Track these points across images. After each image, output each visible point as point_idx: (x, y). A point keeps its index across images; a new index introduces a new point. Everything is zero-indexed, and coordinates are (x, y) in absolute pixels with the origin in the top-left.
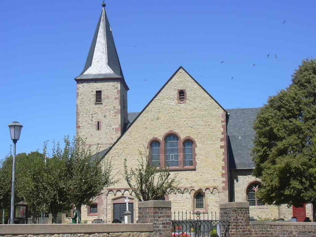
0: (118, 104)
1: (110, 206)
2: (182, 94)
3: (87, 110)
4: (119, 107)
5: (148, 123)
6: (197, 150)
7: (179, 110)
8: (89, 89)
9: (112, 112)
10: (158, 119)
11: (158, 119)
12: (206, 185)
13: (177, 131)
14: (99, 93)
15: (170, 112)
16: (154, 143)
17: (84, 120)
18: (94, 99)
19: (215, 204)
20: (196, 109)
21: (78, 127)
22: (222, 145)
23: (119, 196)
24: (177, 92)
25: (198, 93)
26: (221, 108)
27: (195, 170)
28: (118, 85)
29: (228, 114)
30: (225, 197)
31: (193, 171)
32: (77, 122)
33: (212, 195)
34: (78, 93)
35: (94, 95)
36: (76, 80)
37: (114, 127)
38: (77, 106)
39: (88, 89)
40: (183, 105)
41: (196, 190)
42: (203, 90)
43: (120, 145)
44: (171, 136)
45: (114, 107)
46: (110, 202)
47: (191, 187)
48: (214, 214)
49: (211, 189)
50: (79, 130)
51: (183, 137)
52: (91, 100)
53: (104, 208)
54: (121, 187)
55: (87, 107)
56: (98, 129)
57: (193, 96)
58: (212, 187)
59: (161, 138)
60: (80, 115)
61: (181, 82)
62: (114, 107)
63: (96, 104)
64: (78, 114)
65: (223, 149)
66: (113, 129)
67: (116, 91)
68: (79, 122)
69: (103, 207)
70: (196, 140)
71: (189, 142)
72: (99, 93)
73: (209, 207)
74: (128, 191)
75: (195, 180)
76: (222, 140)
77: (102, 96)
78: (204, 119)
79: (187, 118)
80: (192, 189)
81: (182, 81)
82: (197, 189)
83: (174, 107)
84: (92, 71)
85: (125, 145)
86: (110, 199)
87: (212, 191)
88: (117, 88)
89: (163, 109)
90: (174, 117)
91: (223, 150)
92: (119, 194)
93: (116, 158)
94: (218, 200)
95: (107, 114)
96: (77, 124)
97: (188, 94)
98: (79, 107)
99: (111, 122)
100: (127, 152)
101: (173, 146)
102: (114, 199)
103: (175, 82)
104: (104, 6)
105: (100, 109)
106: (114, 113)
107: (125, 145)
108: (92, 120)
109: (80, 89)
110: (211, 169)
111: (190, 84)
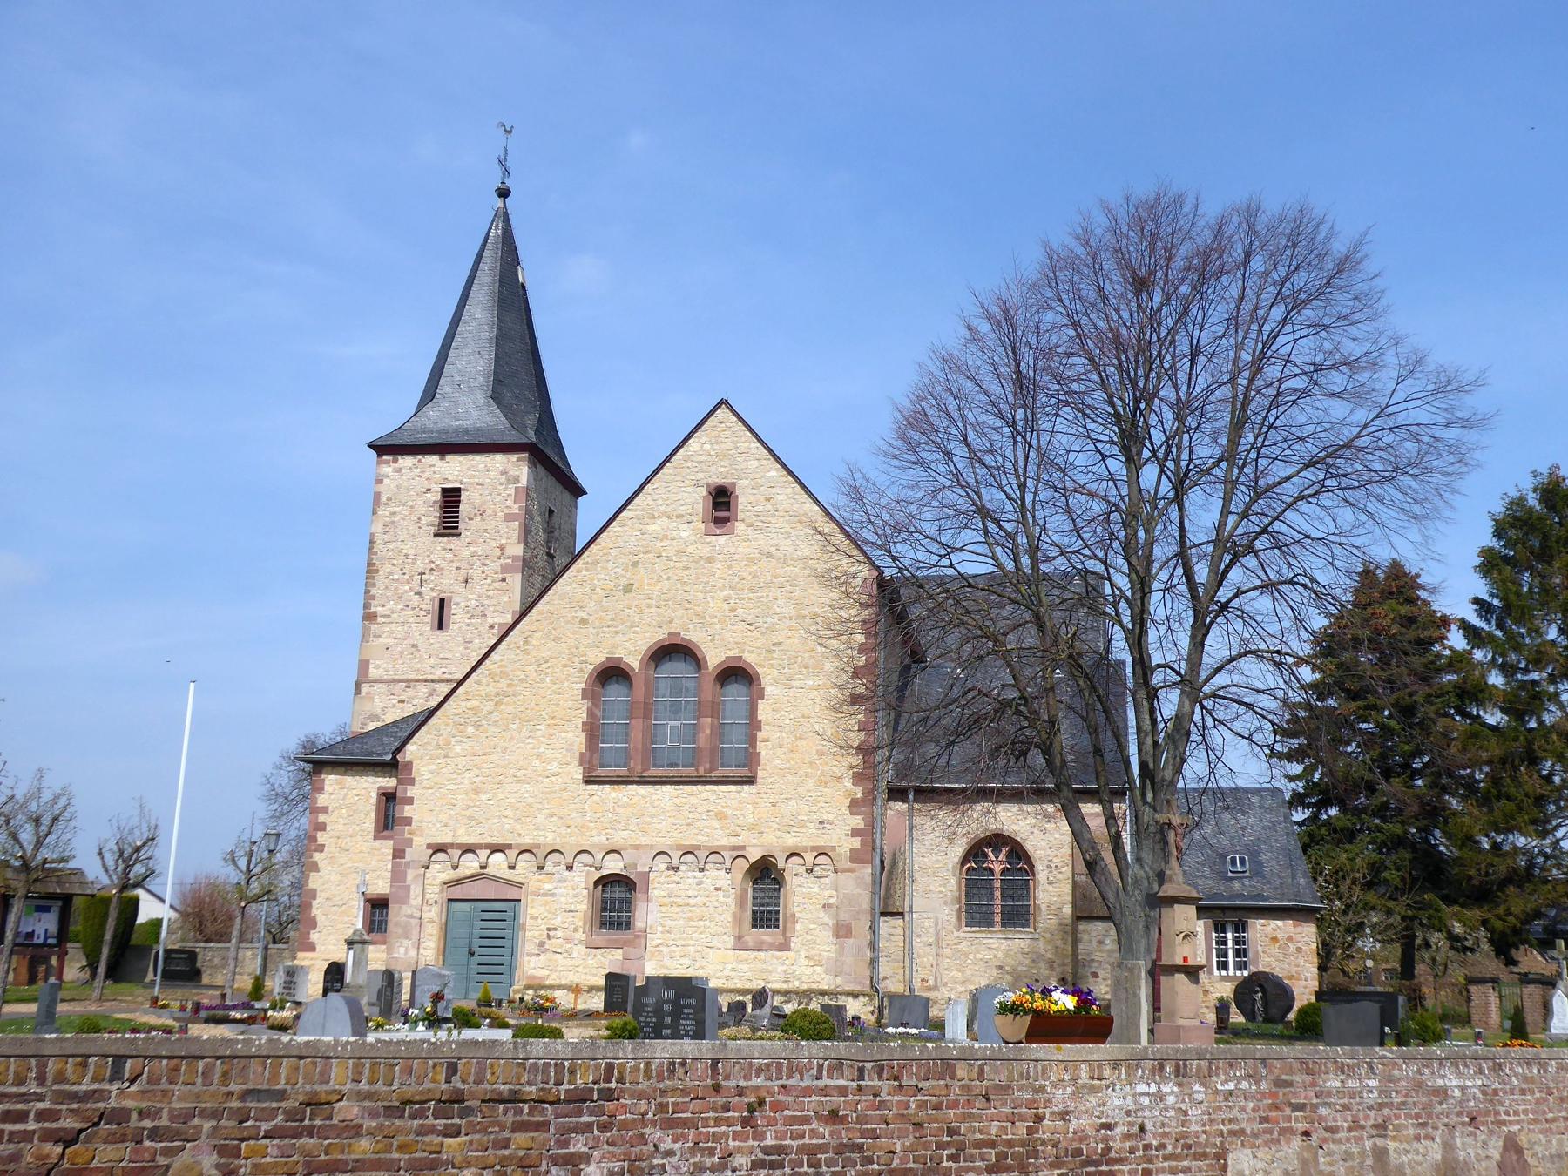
1: (435, 909)
2: (721, 500)
4: (518, 550)
6: (764, 710)
7: (710, 560)
9: (495, 566)
10: (628, 589)
11: (628, 589)
12: (791, 841)
13: (694, 635)
14: (451, 497)
16: (611, 674)
17: (392, 592)
18: (432, 517)
19: (822, 914)
20: (769, 555)
21: (370, 617)
23: (468, 872)
25: (780, 498)
27: (751, 781)
28: (519, 468)
30: (859, 890)
31: (746, 787)
32: (369, 597)
33: (811, 879)
34: (377, 496)
36: (371, 446)
38: (372, 542)
39: (414, 483)
40: (722, 540)
41: (752, 860)
43: (484, 680)
44: (672, 651)
45: (502, 548)
46: (434, 892)
47: (735, 848)
48: (484, 969)
49: (702, 854)
50: (374, 627)
51: (714, 658)
53: (411, 916)
54: (448, 840)
55: (407, 548)
56: (440, 627)
57: (761, 509)
58: (813, 848)
60: (381, 576)
61: (721, 456)
62: (502, 548)
63: (436, 535)
64: (371, 570)
66: (492, 627)
68: (373, 598)
69: (406, 910)
70: (760, 671)
71: (736, 674)
72: (451, 497)
73: (798, 927)
75: (751, 820)
77: (461, 508)
79: (731, 588)
82: (755, 855)
84: (438, 420)
85: (503, 683)
86: (438, 881)
87: (541, 861)
88: (517, 480)
92: (470, 864)
93: (470, 729)
94: (831, 901)
95: (476, 573)
96: (366, 606)
98: (378, 547)
100: (510, 709)
101: (679, 694)
102: (451, 883)
105: (449, 556)
108: (419, 594)
109: (386, 481)
110: (811, 782)
111: (753, 464)
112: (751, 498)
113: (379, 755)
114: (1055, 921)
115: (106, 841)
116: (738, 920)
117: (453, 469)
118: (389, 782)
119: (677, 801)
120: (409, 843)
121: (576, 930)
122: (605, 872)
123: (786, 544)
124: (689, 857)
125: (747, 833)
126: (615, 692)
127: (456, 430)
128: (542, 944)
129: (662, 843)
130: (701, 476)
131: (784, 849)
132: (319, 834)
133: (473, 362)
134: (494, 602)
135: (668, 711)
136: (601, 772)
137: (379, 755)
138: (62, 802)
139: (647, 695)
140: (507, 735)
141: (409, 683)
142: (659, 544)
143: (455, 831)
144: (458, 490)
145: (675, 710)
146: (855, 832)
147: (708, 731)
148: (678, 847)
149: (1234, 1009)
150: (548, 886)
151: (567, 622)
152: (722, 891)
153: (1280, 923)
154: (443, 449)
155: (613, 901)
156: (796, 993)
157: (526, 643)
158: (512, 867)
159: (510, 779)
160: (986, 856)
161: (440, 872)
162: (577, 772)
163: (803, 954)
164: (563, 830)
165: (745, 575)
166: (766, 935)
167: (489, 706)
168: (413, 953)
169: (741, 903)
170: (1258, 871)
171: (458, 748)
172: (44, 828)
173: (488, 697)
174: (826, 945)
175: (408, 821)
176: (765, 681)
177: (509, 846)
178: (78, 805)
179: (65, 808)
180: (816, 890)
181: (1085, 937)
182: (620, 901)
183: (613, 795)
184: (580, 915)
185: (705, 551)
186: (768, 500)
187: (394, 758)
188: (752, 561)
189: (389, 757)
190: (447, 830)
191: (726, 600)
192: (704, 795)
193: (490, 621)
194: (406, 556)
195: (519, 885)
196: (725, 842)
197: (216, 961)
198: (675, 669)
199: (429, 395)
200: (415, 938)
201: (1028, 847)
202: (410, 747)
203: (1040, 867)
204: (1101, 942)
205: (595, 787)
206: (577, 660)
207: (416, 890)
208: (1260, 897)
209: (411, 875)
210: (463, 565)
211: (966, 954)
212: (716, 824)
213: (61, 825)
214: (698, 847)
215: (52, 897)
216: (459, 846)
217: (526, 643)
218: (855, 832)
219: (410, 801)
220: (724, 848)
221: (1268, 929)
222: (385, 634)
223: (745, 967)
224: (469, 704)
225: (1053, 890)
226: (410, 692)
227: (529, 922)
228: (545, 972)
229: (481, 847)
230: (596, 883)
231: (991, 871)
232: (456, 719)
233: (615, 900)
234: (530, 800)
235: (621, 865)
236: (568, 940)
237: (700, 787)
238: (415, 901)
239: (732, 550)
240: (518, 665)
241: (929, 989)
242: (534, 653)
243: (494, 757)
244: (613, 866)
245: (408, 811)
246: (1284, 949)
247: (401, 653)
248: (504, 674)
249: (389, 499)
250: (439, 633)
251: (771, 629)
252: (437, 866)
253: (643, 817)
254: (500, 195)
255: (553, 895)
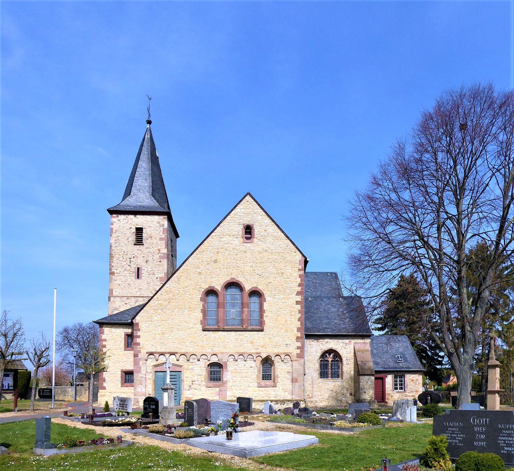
0: (164, 246)
1: (151, 374)
2: (248, 230)
3: (124, 252)
4: (165, 251)
5: (202, 267)
6: (266, 306)
7: (245, 252)
8: (126, 224)
9: (157, 256)
10: (215, 261)
11: (215, 261)
12: (276, 351)
13: (240, 279)
14: (139, 231)
15: (231, 253)
16: (211, 292)
17: (119, 265)
18: (133, 238)
19: (287, 375)
20: (266, 251)
22: (298, 300)
23: (162, 362)
24: (242, 227)
25: (269, 230)
26: (298, 252)
27: (262, 330)
28: (163, 221)
29: (308, 260)
30: (299, 367)
31: (260, 333)
32: (111, 267)
33: (283, 363)
35: (134, 232)
37: (159, 276)
38: (111, 246)
40: (249, 245)
41: (263, 357)
42: (276, 227)
45: (159, 250)
46: (150, 369)
47: (257, 353)
50: (114, 277)
51: (248, 287)
52: (130, 239)
53: (142, 377)
54: (154, 351)
55: (124, 249)
56: (138, 278)
58: (284, 353)
59: (219, 287)
61: (248, 214)
62: (159, 250)
63: (135, 245)
64: (111, 256)
65: (300, 306)
66: (157, 278)
67: (162, 230)
68: (113, 266)
69: (140, 375)
70: (264, 292)
71: (256, 293)
72: (139, 231)
73: (279, 379)
74: (164, 355)
75: (262, 344)
76: (298, 294)
77: (144, 235)
78: (277, 265)
80: (258, 355)
81: (248, 211)
82: (264, 356)
83: (238, 248)
84: (131, 202)
85: (171, 295)
86: (151, 365)
89: (222, 248)
90: (236, 260)
91: (299, 307)
93: (160, 311)
95: (150, 259)
96: (110, 269)
97: (257, 230)
99: (155, 269)
100: (174, 304)
101: (234, 300)
102: (156, 366)
103: (241, 214)
104: (149, 122)
105: (140, 252)
106: (158, 258)
107: (171, 295)
108: (130, 266)
109: (114, 224)
110: (283, 331)
111: (260, 217)
112: (259, 230)
113: (126, 321)
114: (348, 376)
115: (29, 349)
116: (258, 377)
117: (140, 220)
118: (129, 331)
119: (236, 337)
120: (140, 352)
121: (202, 381)
122: (211, 362)
123: (272, 247)
124: (241, 357)
125: (261, 348)
126: (212, 299)
127: (140, 206)
128: (190, 386)
129: (232, 352)
130: (241, 221)
131: (274, 354)
132: (104, 349)
133: (143, 182)
134: (157, 269)
135: (232, 305)
136: (207, 327)
137: (126, 321)
138: (18, 326)
139: (224, 300)
140: (173, 314)
141: (128, 297)
142: (226, 245)
143: (156, 347)
144: (142, 229)
145: (233, 305)
146: (298, 348)
147: (246, 313)
148: (237, 353)
149: (418, 402)
150: (191, 367)
151: (193, 273)
152: (254, 368)
153: (414, 375)
154: (135, 213)
155: (214, 371)
156: (280, 401)
157: (179, 280)
158: (178, 360)
159: (174, 328)
160: (326, 356)
161: (152, 362)
162: (200, 327)
163: (281, 388)
164: (196, 347)
165: (258, 258)
166: (268, 382)
167: (166, 303)
168: (144, 390)
169: (259, 371)
170: (406, 360)
171: (155, 318)
172: (9, 339)
173: (165, 300)
174: (289, 385)
175: (139, 344)
176: (266, 296)
177: (177, 353)
178: (26, 328)
179: (19, 330)
180: (285, 367)
181: (362, 381)
182: (217, 372)
183: (213, 335)
184: (203, 376)
185: (243, 248)
186: (265, 231)
187: (132, 322)
188: (260, 253)
189: (130, 321)
190: (153, 347)
191: (251, 267)
192: (246, 335)
193: (156, 276)
194: (124, 252)
195: (181, 366)
196: (253, 351)
197: (59, 392)
198: (233, 291)
199: (128, 192)
200: (144, 385)
201: (340, 353)
202: (137, 317)
203: (344, 359)
204: (367, 382)
205: (207, 332)
206: (198, 287)
207: (143, 369)
208: (408, 368)
209: (141, 363)
210: (145, 256)
211: (321, 387)
212: (250, 345)
213: (18, 337)
214: (244, 353)
215: (11, 370)
216: (158, 353)
217: (179, 280)
218: (298, 348)
219: (139, 337)
220: (253, 353)
221: (411, 377)
222: (118, 280)
223: (262, 393)
224: (159, 302)
225: (348, 367)
226: (129, 301)
227: (185, 379)
228: (191, 396)
229: (166, 353)
230: (208, 365)
231: (328, 361)
232: (154, 307)
233: (216, 371)
234: (183, 337)
235: (217, 359)
236: (199, 385)
237: (244, 332)
238: (143, 372)
239: (253, 248)
240: (176, 288)
241: (310, 398)
242: (182, 284)
243: (169, 321)
244: (214, 359)
245: (138, 340)
246: (415, 383)
247: (125, 287)
248: (171, 292)
249: (116, 231)
250: (138, 280)
251: (268, 278)
252: (150, 360)
253: (225, 344)
254: (148, 123)
255: (193, 370)
